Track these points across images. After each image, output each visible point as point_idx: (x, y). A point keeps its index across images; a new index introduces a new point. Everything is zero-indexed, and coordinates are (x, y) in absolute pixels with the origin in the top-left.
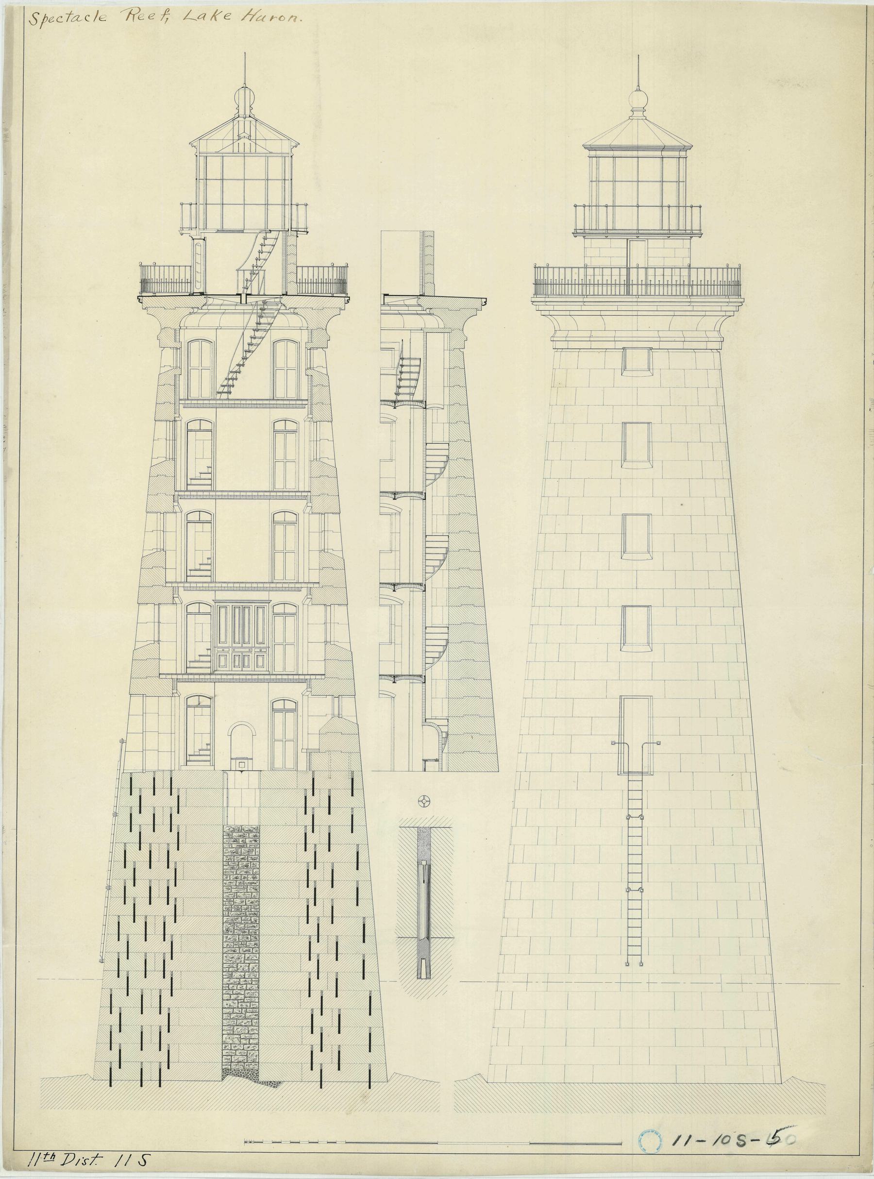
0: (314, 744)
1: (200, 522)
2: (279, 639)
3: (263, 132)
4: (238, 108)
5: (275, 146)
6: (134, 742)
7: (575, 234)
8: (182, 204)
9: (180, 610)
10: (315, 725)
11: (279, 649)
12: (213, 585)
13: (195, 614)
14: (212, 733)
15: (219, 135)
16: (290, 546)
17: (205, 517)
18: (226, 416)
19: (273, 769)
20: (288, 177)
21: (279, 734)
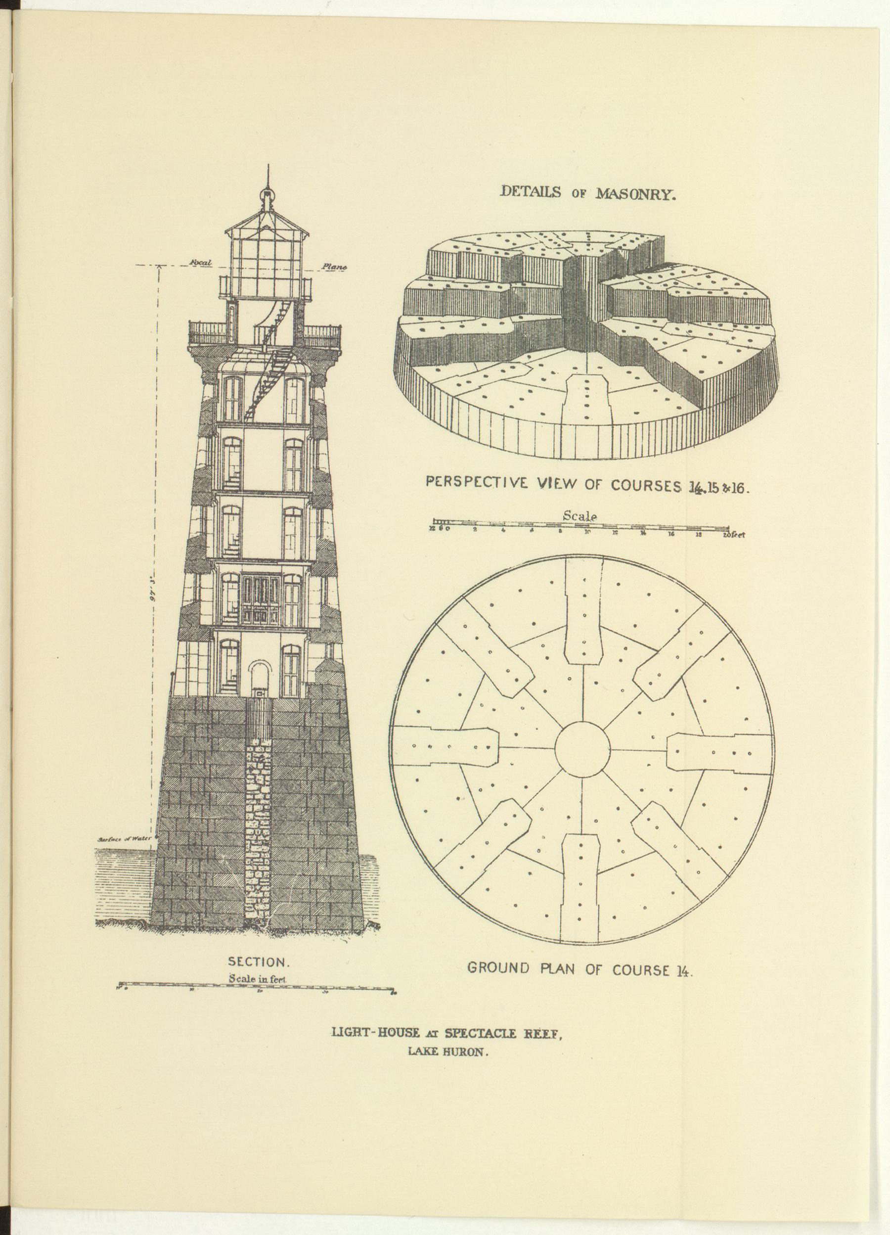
0: (312, 678)
1: (232, 446)
2: (289, 600)
3: (280, 224)
4: (264, 206)
5: (288, 235)
6: (181, 676)
7: (744, 534)
8: (220, 277)
9: (214, 646)
10: (313, 664)
11: (288, 608)
12: (239, 559)
13: (229, 514)
14: (239, 669)
15: (250, 225)
16: (290, 474)
17: (236, 442)
18: (252, 436)
19: (281, 698)
20: (297, 257)
21: (287, 670)
